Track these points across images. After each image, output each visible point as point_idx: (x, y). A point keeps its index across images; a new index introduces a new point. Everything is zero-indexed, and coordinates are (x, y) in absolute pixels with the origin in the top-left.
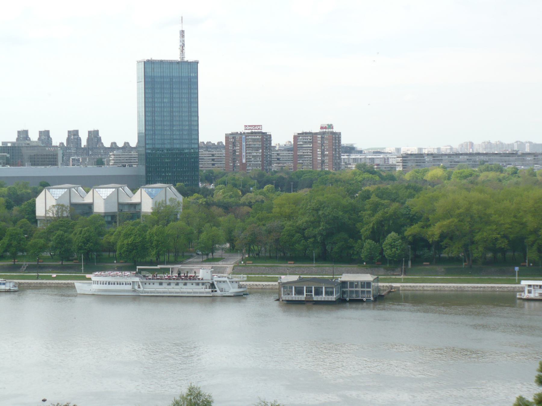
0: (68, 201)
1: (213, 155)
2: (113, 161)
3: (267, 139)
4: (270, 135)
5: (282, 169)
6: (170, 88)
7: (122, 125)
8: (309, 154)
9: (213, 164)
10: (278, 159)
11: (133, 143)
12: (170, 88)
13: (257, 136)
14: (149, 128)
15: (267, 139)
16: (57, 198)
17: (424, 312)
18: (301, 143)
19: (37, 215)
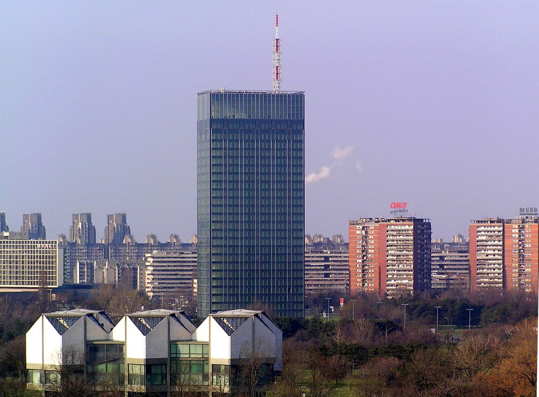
0: (82, 338)
1: (327, 259)
2: (151, 268)
3: (422, 230)
4: (429, 224)
5: (448, 284)
6: (257, 142)
7: (170, 201)
8: (497, 256)
9: (327, 275)
10: (442, 266)
11: (190, 236)
12: (257, 142)
13: (405, 225)
14: (229, 306)
15: (422, 230)
16: (483, 310)
17: (284, 349)
18: (484, 238)
19: (28, 361)
